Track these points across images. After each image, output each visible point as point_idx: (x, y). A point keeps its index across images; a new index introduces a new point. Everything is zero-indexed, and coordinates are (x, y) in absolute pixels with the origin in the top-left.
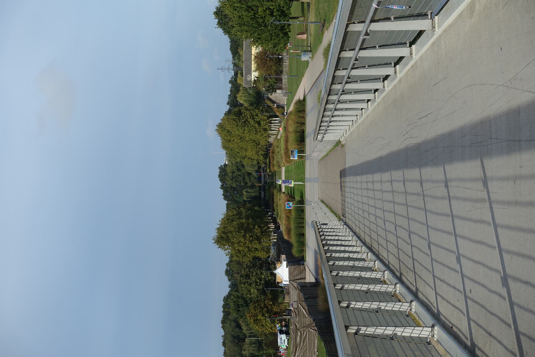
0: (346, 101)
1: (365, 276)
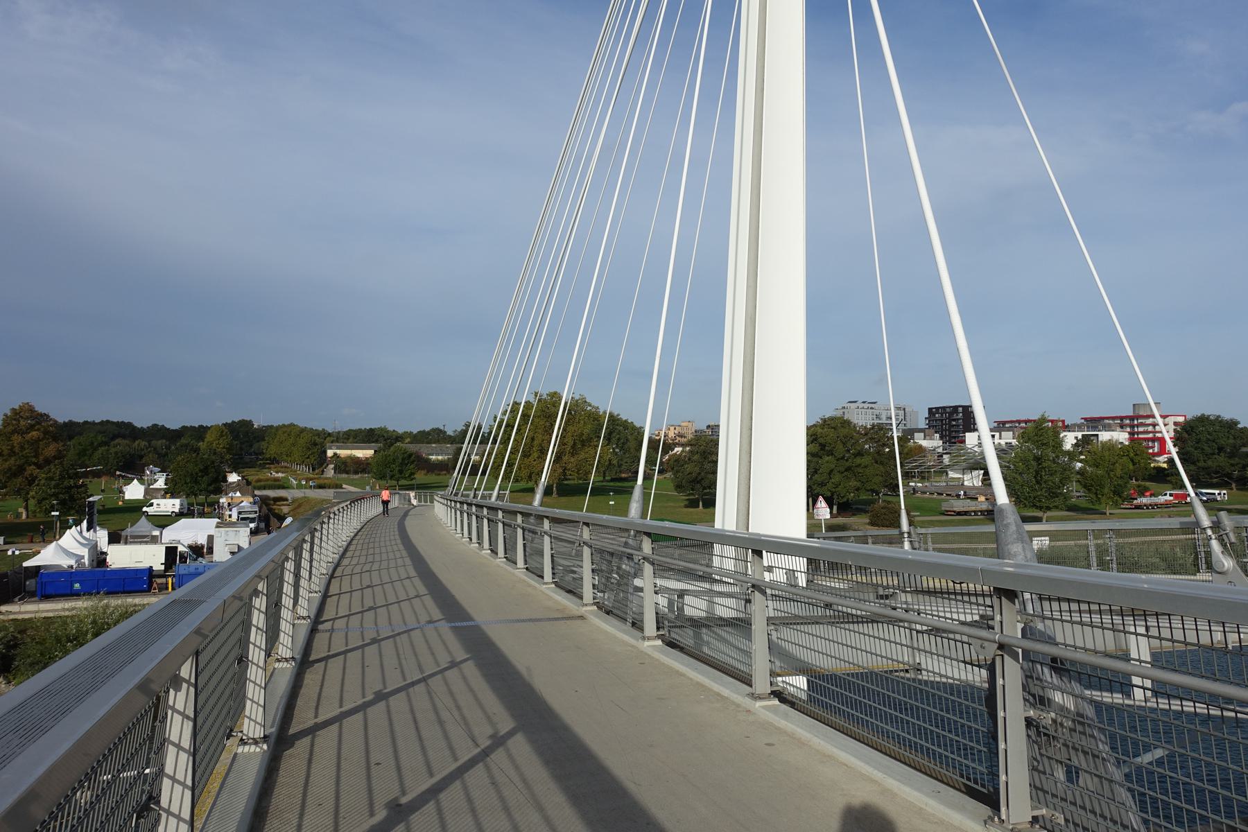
0: (1111, 516)
1: (251, 645)
